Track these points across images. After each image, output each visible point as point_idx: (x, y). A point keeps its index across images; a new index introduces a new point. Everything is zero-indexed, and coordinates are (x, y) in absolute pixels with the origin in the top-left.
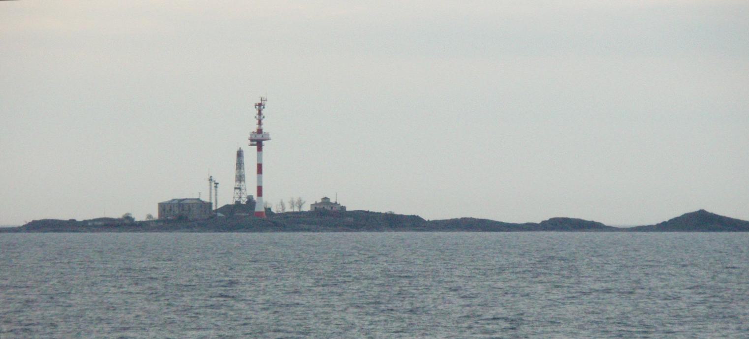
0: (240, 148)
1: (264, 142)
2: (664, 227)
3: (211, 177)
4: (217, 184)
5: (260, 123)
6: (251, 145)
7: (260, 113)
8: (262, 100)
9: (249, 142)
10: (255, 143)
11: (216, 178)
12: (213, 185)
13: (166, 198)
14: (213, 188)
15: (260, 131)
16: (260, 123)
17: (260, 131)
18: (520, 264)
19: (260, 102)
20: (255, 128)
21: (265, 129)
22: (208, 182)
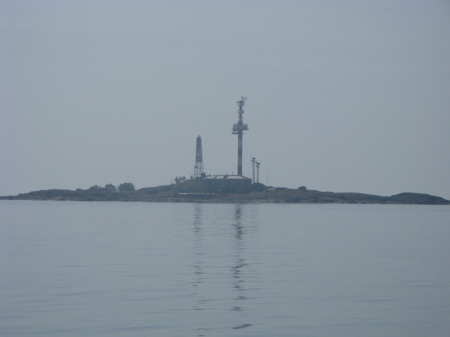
0: (199, 136)
1: (243, 131)
2: (22, 197)
3: (254, 158)
4: (259, 164)
5: (241, 117)
6: (233, 133)
7: (241, 109)
8: (242, 99)
9: (232, 131)
10: (237, 132)
11: (258, 160)
12: (256, 164)
13: (179, 176)
14: (256, 168)
15: (240, 122)
16: (241, 117)
17: (240, 122)
18: (240, 226)
19: (241, 100)
20: (236, 121)
21: (245, 122)
22: (251, 163)
